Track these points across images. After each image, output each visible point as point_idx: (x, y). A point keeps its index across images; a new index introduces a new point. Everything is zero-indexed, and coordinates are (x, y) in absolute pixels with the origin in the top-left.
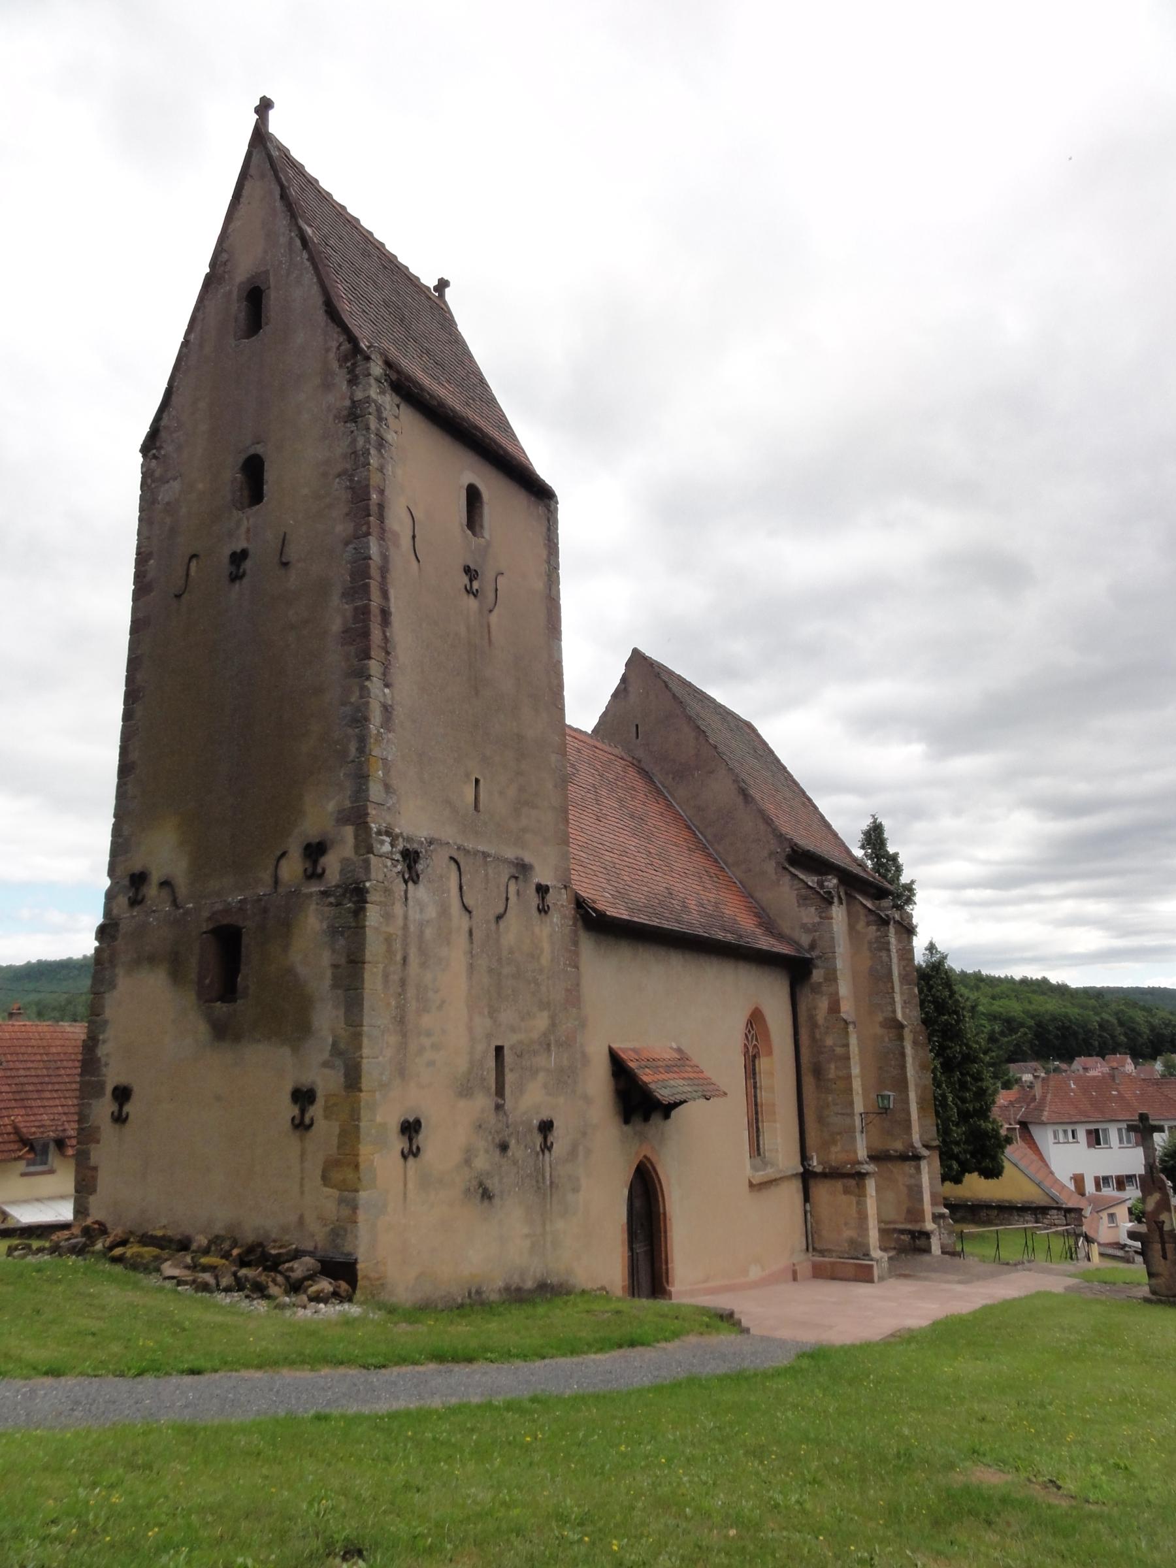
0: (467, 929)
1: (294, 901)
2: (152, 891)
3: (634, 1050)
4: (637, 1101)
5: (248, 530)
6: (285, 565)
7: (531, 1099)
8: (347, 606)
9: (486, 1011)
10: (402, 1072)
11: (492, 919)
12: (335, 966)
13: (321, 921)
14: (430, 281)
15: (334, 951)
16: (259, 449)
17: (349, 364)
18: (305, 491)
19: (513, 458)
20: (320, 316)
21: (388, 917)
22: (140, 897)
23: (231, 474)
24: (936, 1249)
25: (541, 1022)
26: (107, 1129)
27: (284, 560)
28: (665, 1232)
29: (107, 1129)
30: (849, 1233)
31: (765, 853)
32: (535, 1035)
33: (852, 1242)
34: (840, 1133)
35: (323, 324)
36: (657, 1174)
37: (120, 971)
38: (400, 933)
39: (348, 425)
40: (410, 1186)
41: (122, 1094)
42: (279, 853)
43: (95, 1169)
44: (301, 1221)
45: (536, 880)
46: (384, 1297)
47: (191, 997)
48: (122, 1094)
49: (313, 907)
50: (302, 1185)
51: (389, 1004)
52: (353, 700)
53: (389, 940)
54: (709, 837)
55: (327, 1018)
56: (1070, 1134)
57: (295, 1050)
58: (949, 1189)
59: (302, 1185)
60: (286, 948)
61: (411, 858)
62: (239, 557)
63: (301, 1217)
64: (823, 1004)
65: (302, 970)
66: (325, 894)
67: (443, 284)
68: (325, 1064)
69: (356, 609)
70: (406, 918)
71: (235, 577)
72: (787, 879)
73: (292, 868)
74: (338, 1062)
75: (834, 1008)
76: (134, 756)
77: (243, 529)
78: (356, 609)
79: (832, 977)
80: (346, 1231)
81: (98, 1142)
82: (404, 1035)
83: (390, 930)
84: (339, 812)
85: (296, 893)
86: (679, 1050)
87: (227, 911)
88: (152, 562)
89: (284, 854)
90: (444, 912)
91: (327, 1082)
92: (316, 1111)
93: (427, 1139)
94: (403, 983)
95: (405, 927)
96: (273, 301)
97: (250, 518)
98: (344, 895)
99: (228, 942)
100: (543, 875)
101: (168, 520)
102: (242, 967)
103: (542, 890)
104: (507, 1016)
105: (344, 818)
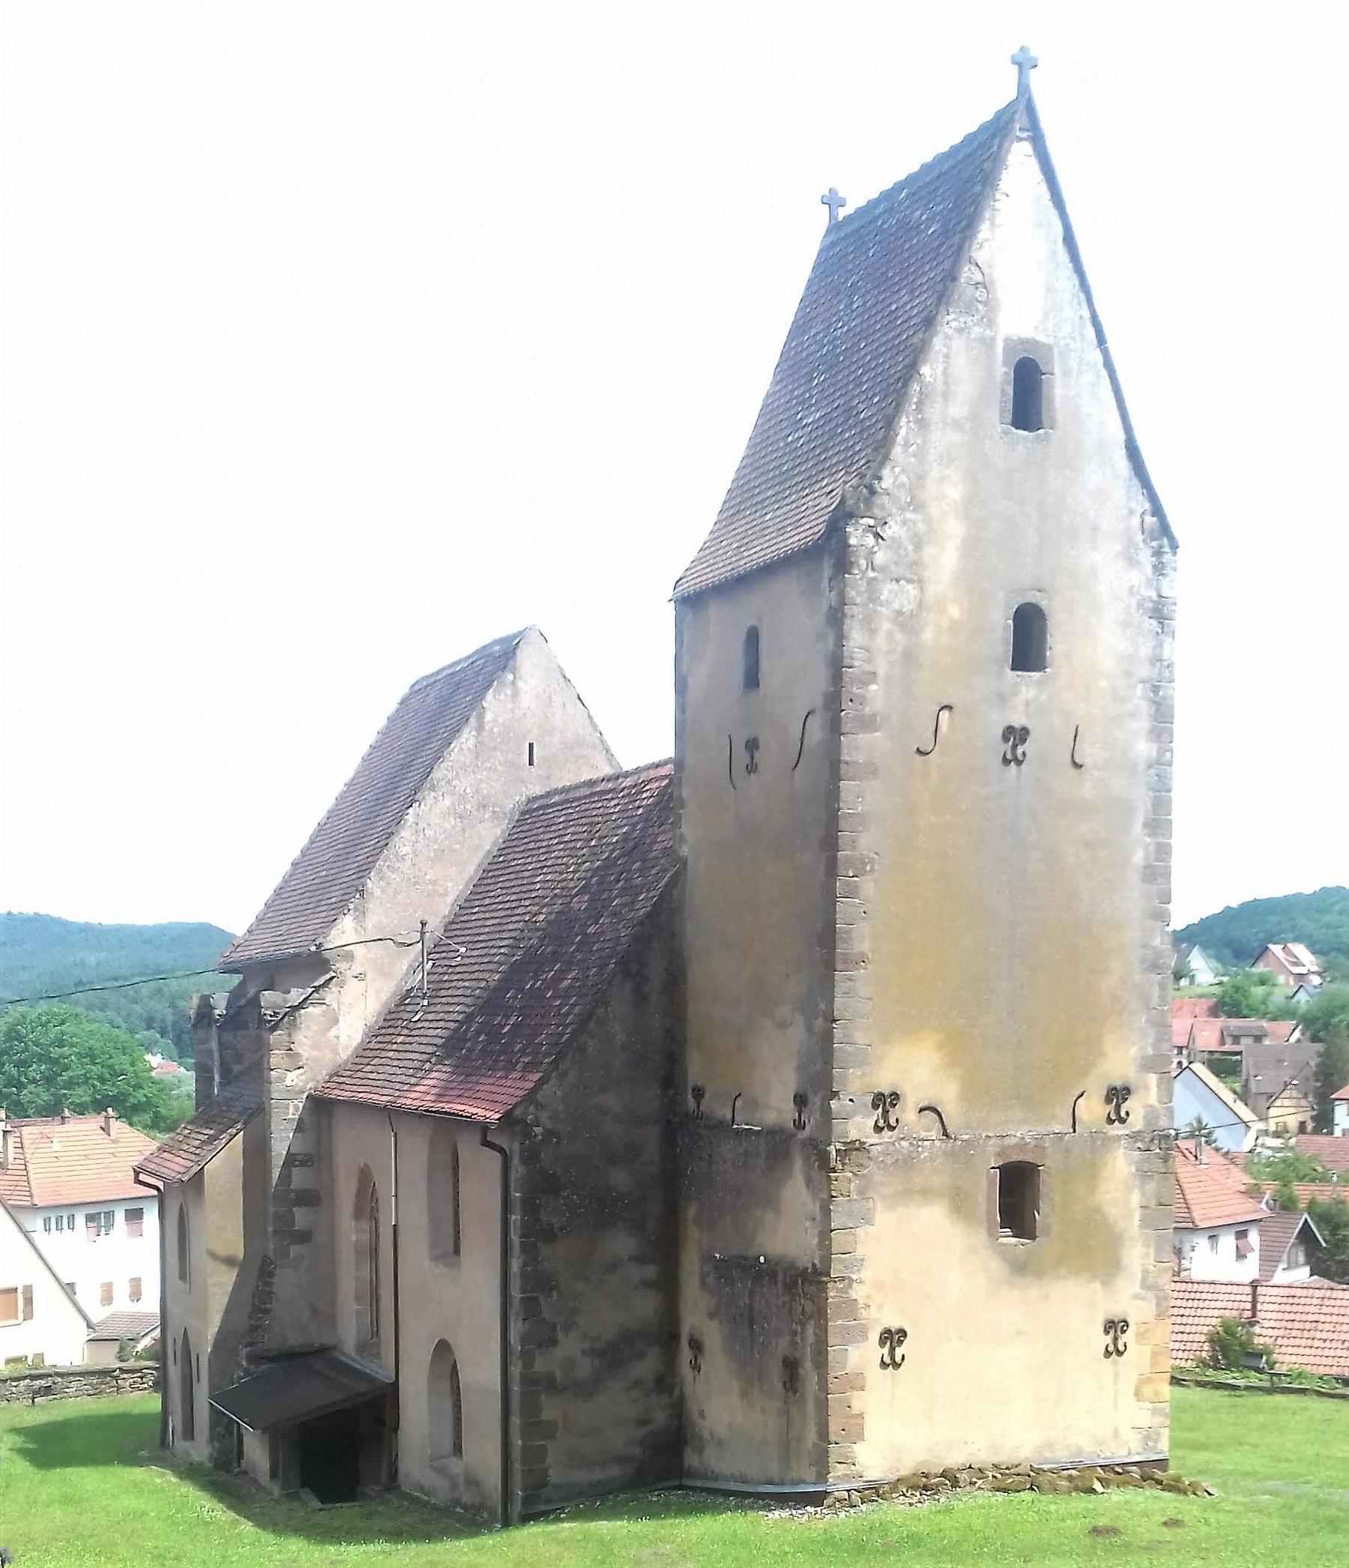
1: (1099, 1143)
5: (1027, 704)
6: (1077, 766)
8: (1148, 839)
15: (1143, 1194)
17: (1154, 544)
18: (1103, 683)
26: (874, 1374)
41: (893, 1338)
42: (1079, 1093)
43: (861, 1416)
44: (1116, 1433)
46: (894, 1536)
47: (982, 1234)
48: (893, 1338)
49: (1122, 1150)
50: (1115, 1403)
56: (65, 1221)
57: (1105, 1284)
59: (1115, 1403)
60: (1092, 1189)
62: (1015, 735)
63: (1116, 1430)
65: (1112, 1212)
66: (1135, 1136)
68: (1136, 1297)
71: (1012, 759)
73: (1093, 1109)
74: (1150, 1295)
84: (1143, 1058)
85: (1093, 1135)
87: (1022, 1146)
88: (874, 687)
91: (1137, 1310)
97: (1027, 686)
101: (899, 636)
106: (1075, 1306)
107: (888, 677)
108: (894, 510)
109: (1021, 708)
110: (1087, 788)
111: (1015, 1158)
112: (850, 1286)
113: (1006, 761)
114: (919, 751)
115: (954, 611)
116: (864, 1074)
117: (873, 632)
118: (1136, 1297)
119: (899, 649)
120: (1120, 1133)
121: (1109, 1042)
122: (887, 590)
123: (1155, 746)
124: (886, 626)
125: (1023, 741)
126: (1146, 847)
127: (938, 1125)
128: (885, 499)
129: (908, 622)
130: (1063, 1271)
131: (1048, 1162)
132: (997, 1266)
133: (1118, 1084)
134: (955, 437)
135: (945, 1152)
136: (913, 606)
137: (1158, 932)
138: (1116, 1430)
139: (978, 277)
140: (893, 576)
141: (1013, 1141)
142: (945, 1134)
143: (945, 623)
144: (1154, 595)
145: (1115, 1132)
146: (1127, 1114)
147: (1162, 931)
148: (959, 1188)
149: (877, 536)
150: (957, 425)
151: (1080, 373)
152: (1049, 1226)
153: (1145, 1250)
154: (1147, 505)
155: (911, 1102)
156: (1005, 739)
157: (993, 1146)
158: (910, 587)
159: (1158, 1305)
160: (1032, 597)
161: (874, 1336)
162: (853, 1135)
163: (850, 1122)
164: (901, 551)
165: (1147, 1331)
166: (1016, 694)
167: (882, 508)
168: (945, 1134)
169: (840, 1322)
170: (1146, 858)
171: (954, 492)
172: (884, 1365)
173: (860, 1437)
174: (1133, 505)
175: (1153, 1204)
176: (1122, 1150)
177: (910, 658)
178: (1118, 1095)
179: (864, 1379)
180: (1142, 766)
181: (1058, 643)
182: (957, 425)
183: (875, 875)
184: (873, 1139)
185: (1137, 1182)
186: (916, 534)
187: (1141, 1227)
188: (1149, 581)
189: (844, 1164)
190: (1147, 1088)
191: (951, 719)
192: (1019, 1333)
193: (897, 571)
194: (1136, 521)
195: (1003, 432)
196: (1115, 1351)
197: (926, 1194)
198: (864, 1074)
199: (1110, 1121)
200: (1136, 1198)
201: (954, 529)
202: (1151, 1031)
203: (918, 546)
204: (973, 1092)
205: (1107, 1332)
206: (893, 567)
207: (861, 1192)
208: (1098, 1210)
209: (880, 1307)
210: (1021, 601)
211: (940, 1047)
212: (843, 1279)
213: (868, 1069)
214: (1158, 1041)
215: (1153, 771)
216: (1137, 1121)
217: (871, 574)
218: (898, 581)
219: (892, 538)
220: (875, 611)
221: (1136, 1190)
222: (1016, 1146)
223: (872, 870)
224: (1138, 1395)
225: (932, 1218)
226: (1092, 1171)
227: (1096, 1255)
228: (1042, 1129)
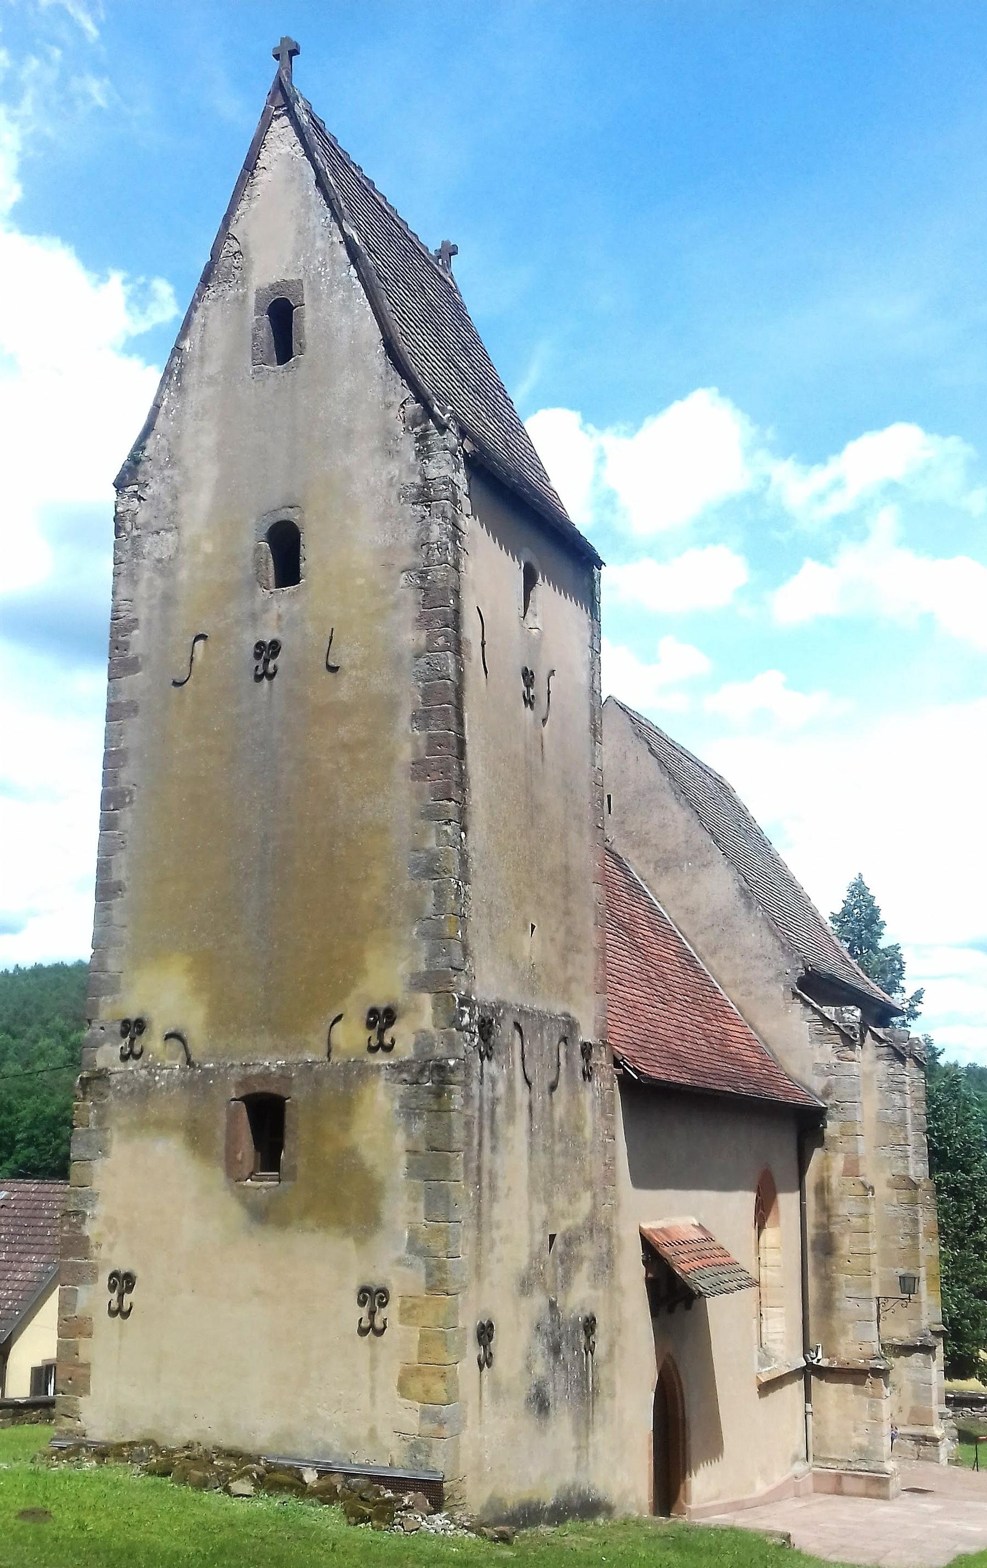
0: (526, 1103)
1: (356, 1073)
2: (153, 1042)
3: (662, 1230)
4: (673, 1295)
5: (279, 617)
7: (580, 1296)
9: (542, 1195)
10: (478, 1271)
11: (546, 1087)
12: (412, 1152)
13: (392, 1100)
14: (433, 246)
15: (409, 1136)
16: (294, 516)
17: (417, 429)
18: (361, 581)
19: (536, 493)
20: (377, 358)
21: (468, 1098)
22: (137, 1049)
23: (252, 542)
24: (943, 1457)
25: (585, 1204)
27: (332, 663)
28: (684, 1441)
29: (102, 1320)
30: (859, 1440)
31: (771, 973)
32: (580, 1220)
33: (861, 1450)
34: (852, 1321)
35: (381, 370)
36: (678, 1376)
37: (114, 1136)
38: (477, 1114)
39: (418, 508)
40: (485, 1395)
41: (123, 1282)
43: (87, 1366)
44: (373, 1433)
45: (581, 1039)
47: (220, 1173)
48: (123, 1282)
49: (382, 1083)
51: (468, 1195)
52: (428, 846)
53: (468, 1125)
54: (699, 948)
55: (402, 1210)
58: (948, 1384)
59: (372, 1396)
60: (345, 1127)
61: (486, 1028)
62: (268, 650)
63: (373, 1431)
64: (838, 1163)
65: (369, 1156)
66: (398, 1068)
67: (450, 251)
68: (400, 1261)
69: (430, 737)
70: (481, 1097)
72: (799, 1005)
73: (351, 1035)
74: (419, 1262)
75: (852, 1169)
76: (120, 874)
77: (272, 615)
78: (430, 737)
79: (850, 1133)
80: (430, 1447)
81: (90, 1335)
82: (479, 1227)
83: (469, 1112)
84: (413, 975)
86: (700, 1227)
87: (266, 1076)
88: (136, 632)
89: (339, 1018)
90: (511, 1088)
91: (403, 1280)
92: (390, 1313)
93: (500, 1345)
94: (479, 1169)
95: (481, 1109)
96: (308, 321)
97: (282, 602)
98: (421, 1072)
99: (266, 1118)
100: (587, 1035)
101: (159, 582)
102: (287, 1142)
103: (586, 1050)
104: (560, 1202)
105: (420, 982)
106: (325, 1266)
107: (149, 622)
108: (155, 472)
109: (274, 623)
110: (344, 690)
111: (258, 1089)
112: (83, 1221)
113: (258, 678)
114: (176, 684)
115: (208, 547)
116: (114, 1002)
117: (135, 583)
118: (400, 1261)
119: (159, 593)
120: (381, 1062)
121: (372, 958)
122: (148, 544)
123: (424, 634)
124: (146, 575)
125: (275, 655)
126: (415, 740)
127: (182, 1053)
128: (148, 464)
129: (164, 567)
130: (310, 1222)
131: (295, 1094)
132: (236, 1212)
133: (382, 1005)
134: (208, 391)
135: (183, 1083)
136: (172, 552)
137: (433, 831)
138: (373, 1431)
139: (236, 247)
140: (154, 529)
141: (255, 1071)
142: (189, 1062)
143: (200, 558)
144: (418, 480)
145: (377, 1062)
146: (393, 1041)
147: (438, 832)
148: (195, 1121)
149: (140, 498)
150: (212, 381)
151: (330, 294)
152: (294, 1168)
153: (412, 1205)
154: (408, 393)
155: (157, 1029)
156: (257, 656)
157: (234, 1076)
158: (169, 535)
159: (429, 1275)
160: (283, 515)
161: (104, 1279)
162: (101, 1063)
163: (99, 1051)
164: (161, 506)
165: (414, 1307)
166: (266, 611)
167: (145, 473)
168: (189, 1062)
169: (71, 1260)
170: (416, 752)
171: (208, 440)
172: (112, 1313)
173: (86, 1391)
174: (392, 398)
175: (422, 1147)
176: (382, 1083)
177: (168, 600)
178: (382, 1018)
179: (91, 1324)
180: (408, 656)
181: (311, 555)
182: (212, 381)
183: (134, 806)
184: (120, 1067)
185: (402, 1121)
186: (174, 487)
187: (410, 1175)
188: (411, 469)
189: (85, 1093)
190: (418, 1010)
191: (206, 647)
192: (257, 1293)
193: (156, 524)
194: (394, 413)
195: (255, 372)
196: (371, 1330)
197: (161, 1125)
198: (114, 1002)
199: (372, 1050)
200: (400, 1140)
201: (208, 473)
202: (424, 945)
203: (175, 498)
204: (224, 1017)
205: (362, 1303)
206: (153, 522)
207: (100, 1120)
208: (352, 1152)
209: (111, 1247)
210: (273, 520)
211: (189, 970)
212: (76, 1213)
213: (117, 996)
214: (433, 955)
215: (423, 660)
216: (405, 1048)
217: (135, 533)
218: (158, 533)
219: (153, 497)
220: (138, 564)
221: (400, 1130)
222: (259, 1076)
223: (131, 802)
224: (402, 1388)
225: (167, 1155)
226: (346, 1106)
227: (349, 1203)
228: (292, 1058)
